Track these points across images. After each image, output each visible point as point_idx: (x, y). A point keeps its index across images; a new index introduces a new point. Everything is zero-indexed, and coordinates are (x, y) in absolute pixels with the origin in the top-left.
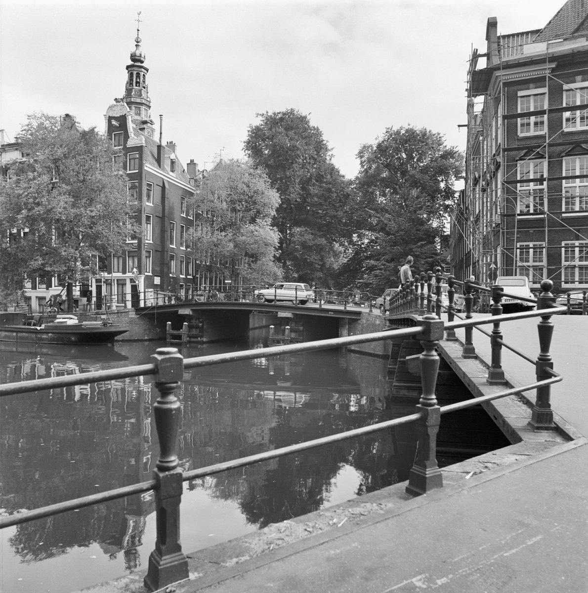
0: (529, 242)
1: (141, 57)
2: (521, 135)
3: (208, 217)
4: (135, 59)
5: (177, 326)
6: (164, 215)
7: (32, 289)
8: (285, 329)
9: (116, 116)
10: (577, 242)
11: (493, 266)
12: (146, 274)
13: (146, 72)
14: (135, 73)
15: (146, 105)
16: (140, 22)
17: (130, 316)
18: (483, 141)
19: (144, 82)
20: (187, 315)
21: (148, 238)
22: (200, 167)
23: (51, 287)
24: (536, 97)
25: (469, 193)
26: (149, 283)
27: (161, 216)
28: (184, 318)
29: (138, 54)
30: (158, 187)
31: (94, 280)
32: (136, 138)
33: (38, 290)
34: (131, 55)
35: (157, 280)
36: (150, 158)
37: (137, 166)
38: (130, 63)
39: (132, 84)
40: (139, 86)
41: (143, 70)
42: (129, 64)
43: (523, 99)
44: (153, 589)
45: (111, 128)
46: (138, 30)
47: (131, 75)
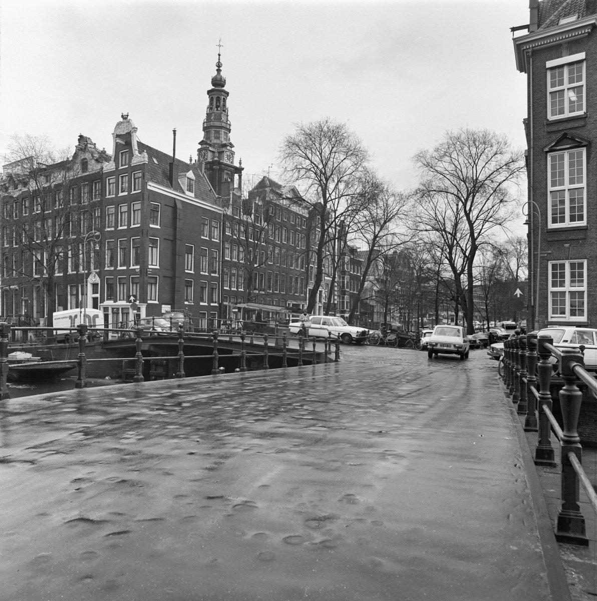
0: (563, 259)
1: (221, 81)
2: (551, 118)
4: (218, 82)
6: (175, 238)
10: (567, 261)
12: (149, 302)
13: (226, 95)
14: (215, 97)
15: (225, 128)
16: (221, 47)
17: (96, 351)
27: (171, 238)
30: (167, 207)
38: (211, 87)
41: (223, 93)
44: (560, 516)
45: (118, 147)
46: (219, 55)
47: (211, 100)
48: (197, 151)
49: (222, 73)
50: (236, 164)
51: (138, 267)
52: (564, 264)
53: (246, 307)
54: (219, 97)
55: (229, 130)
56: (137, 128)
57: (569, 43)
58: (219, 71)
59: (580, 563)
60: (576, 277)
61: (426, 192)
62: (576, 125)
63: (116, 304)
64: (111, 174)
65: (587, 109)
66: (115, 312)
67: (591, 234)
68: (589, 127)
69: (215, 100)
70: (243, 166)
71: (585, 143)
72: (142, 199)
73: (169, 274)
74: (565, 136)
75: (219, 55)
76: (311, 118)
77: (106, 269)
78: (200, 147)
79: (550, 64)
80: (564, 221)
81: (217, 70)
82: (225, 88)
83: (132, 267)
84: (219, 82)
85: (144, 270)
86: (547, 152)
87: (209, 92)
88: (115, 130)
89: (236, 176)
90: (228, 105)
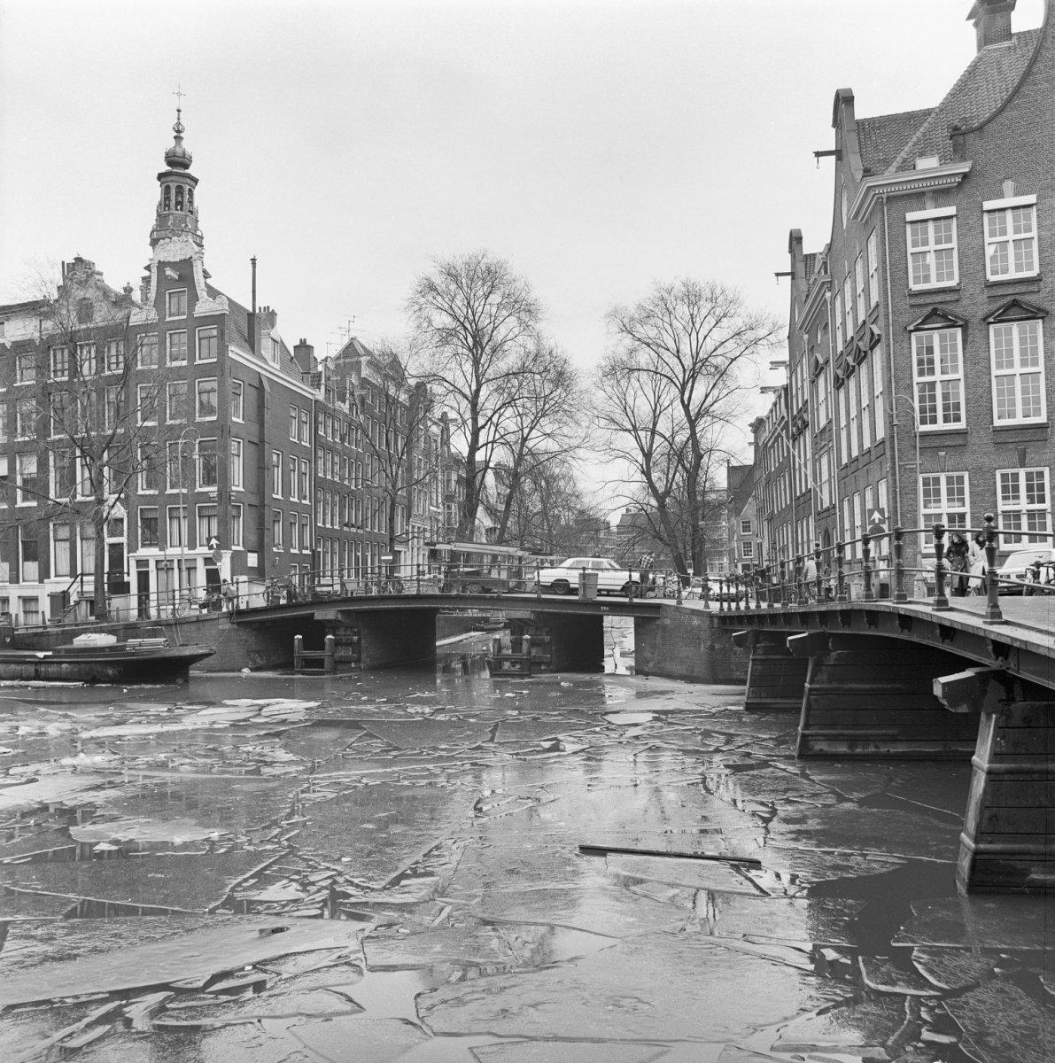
3: (335, 442)
4: (178, 160)
5: (314, 641)
6: (262, 441)
7: (11, 582)
8: (522, 639)
9: (172, 260)
10: (943, 474)
11: (876, 516)
12: (234, 548)
18: (834, 298)
19: (191, 202)
20: (329, 621)
21: (236, 483)
22: (319, 354)
23: (49, 578)
24: (938, 223)
25: (802, 394)
26: (238, 565)
27: (256, 440)
28: (324, 626)
29: (179, 151)
31: (133, 563)
33: (21, 583)
35: (252, 560)
36: (236, 336)
37: (214, 351)
38: (165, 168)
39: (168, 206)
40: (181, 209)
41: (188, 181)
42: (164, 171)
43: (915, 226)
46: (179, 111)
47: (167, 190)
49: (184, 143)
51: (215, 488)
52: (962, 477)
53: (454, 549)
57: (935, 192)
58: (178, 138)
60: (955, 493)
61: (619, 370)
62: (948, 299)
63: (196, 551)
64: (146, 328)
65: (961, 275)
66: (164, 567)
67: (972, 439)
68: (965, 302)
69: (173, 191)
71: (960, 323)
72: (218, 373)
73: (254, 500)
74: (934, 312)
76: (458, 251)
77: (140, 492)
79: (910, 216)
80: (935, 422)
81: (175, 137)
82: (191, 171)
83: (198, 490)
84: (180, 160)
85: (224, 495)
86: (911, 331)
87: (160, 176)
90: (196, 203)
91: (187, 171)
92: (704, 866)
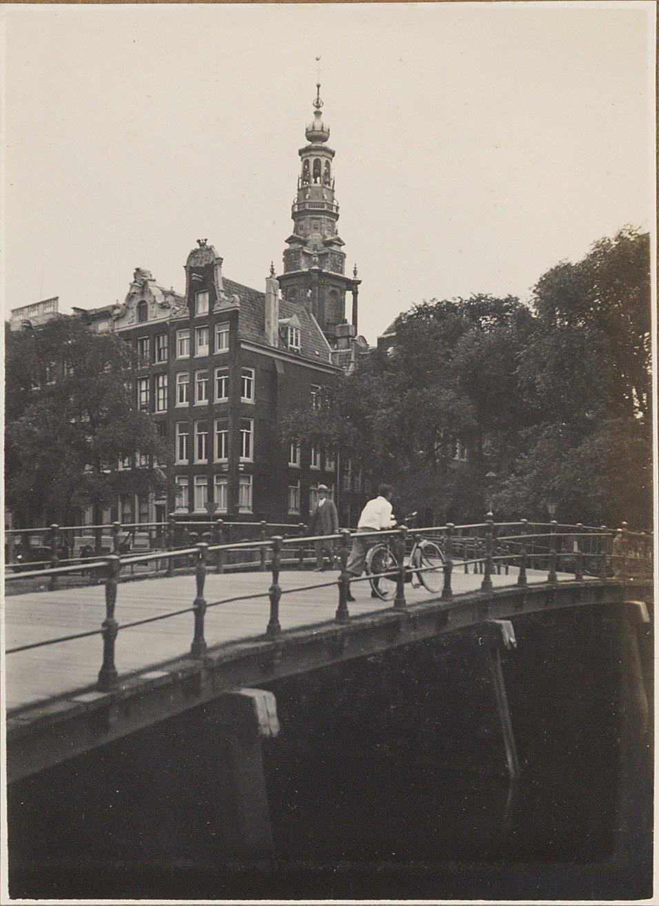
1: (323, 131)
4: (317, 136)
14: (312, 160)
29: (318, 128)
32: (226, 298)
34: (307, 132)
46: (318, 86)
48: (282, 254)
50: (349, 274)
54: (319, 160)
55: (337, 216)
56: (222, 259)
58: (318, 114)
59: (276, 535)
70: (359, 278)
75: (318, 86)
78: (287, 246)
87: (301, 152)
88: (188, 262)
89: (349, 294)
90: (333, 174)
91: (325, 144)
92: (222, 596)
